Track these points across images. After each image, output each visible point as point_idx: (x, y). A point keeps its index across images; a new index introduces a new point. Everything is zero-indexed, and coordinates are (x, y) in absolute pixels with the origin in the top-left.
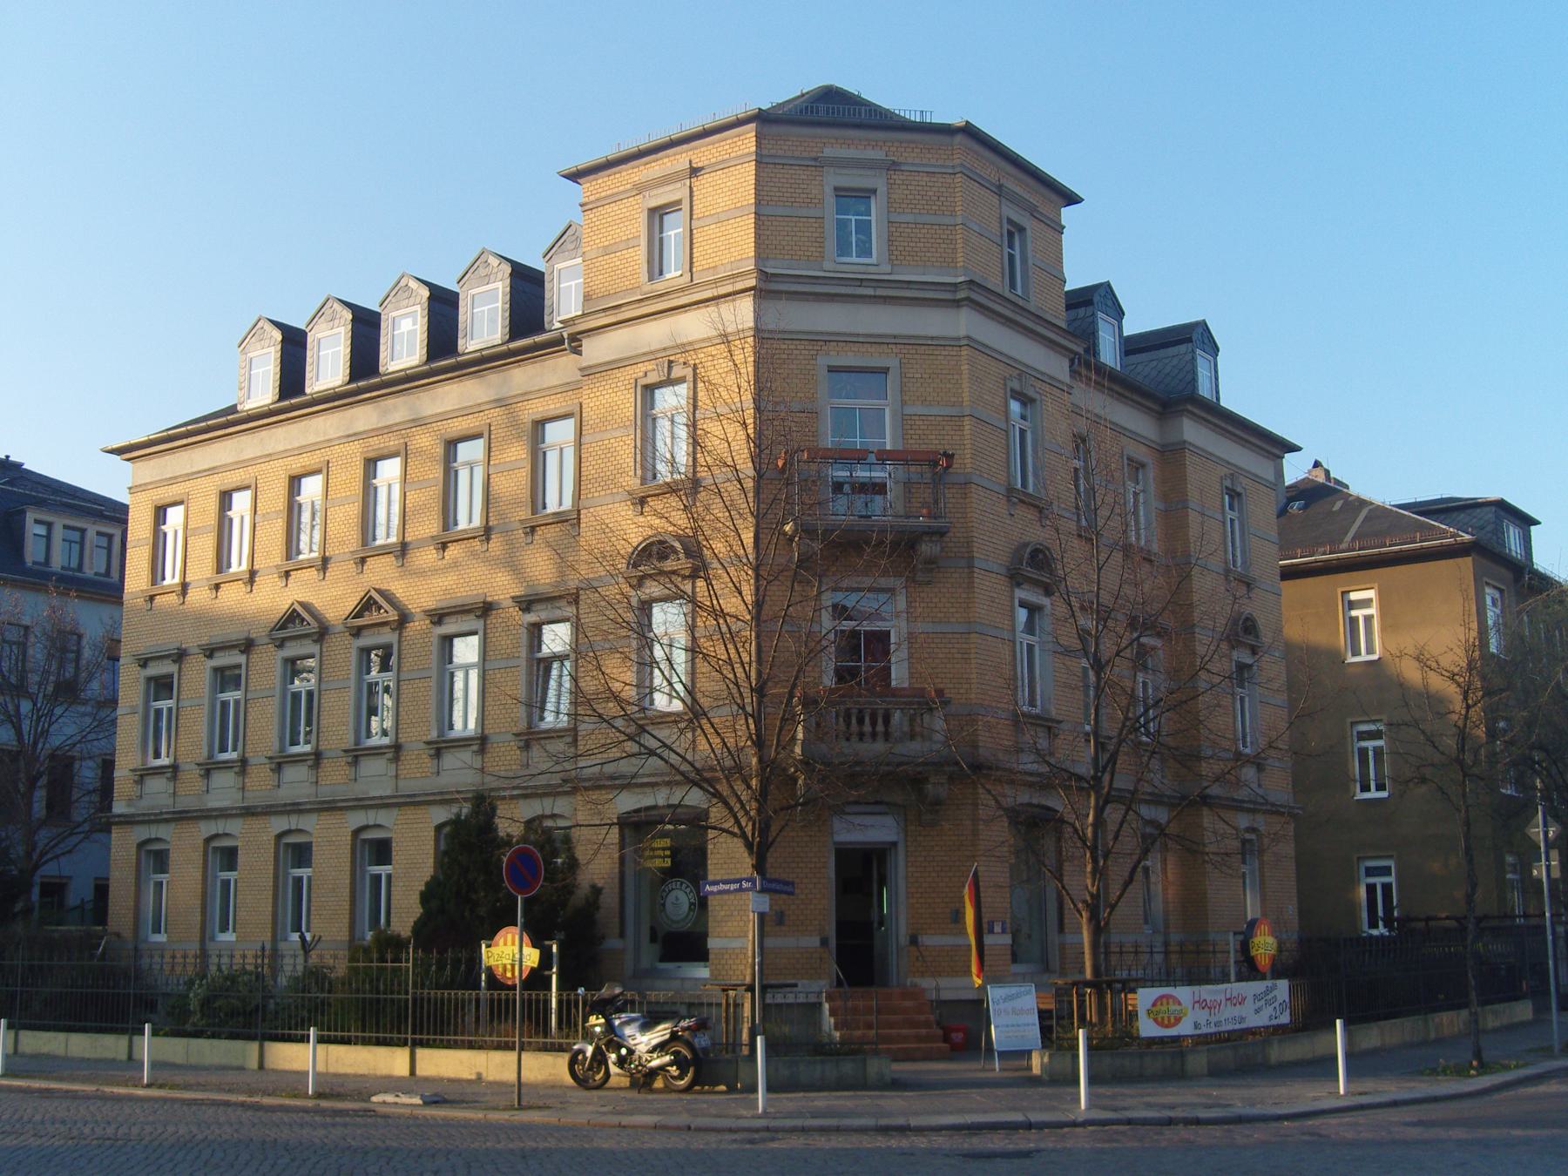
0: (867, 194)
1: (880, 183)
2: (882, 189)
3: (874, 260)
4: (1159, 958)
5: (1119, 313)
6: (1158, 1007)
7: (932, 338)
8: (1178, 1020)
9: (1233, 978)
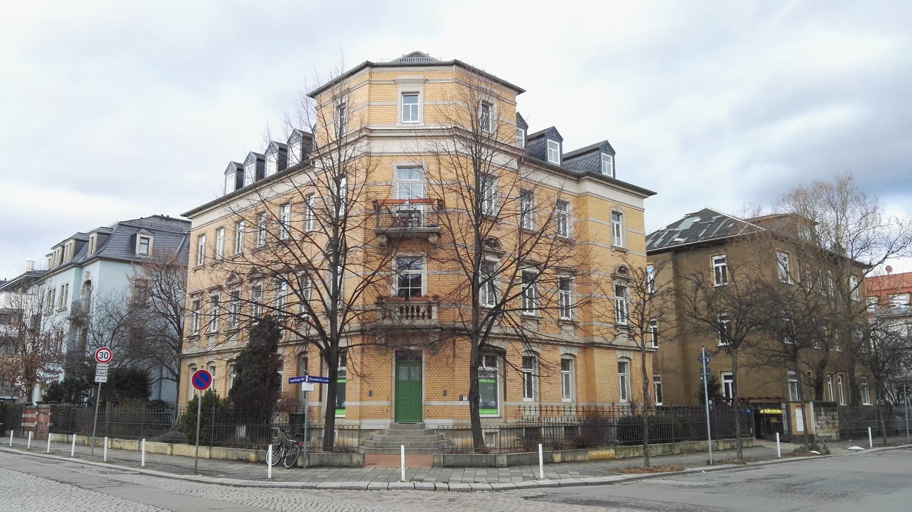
0: (414, 95)
1: (419, 88)
2: (422, 92)
4: (574, 413)
5: (560, 139)
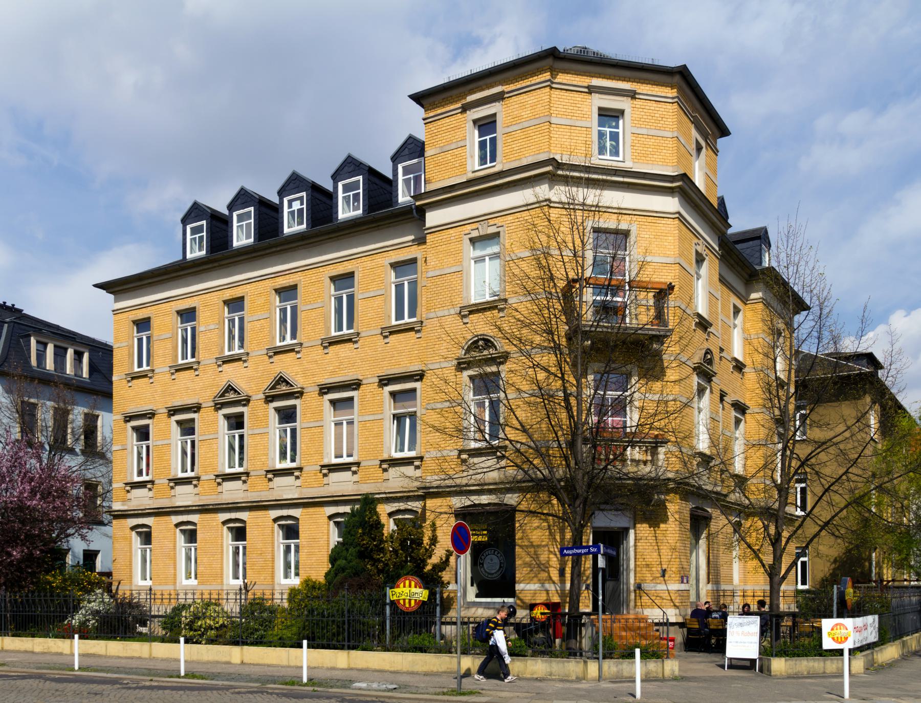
3: (621, 158)
6: (835, 631)
7: (657, 212)
8: (846, 639)
9: (835, 615)
